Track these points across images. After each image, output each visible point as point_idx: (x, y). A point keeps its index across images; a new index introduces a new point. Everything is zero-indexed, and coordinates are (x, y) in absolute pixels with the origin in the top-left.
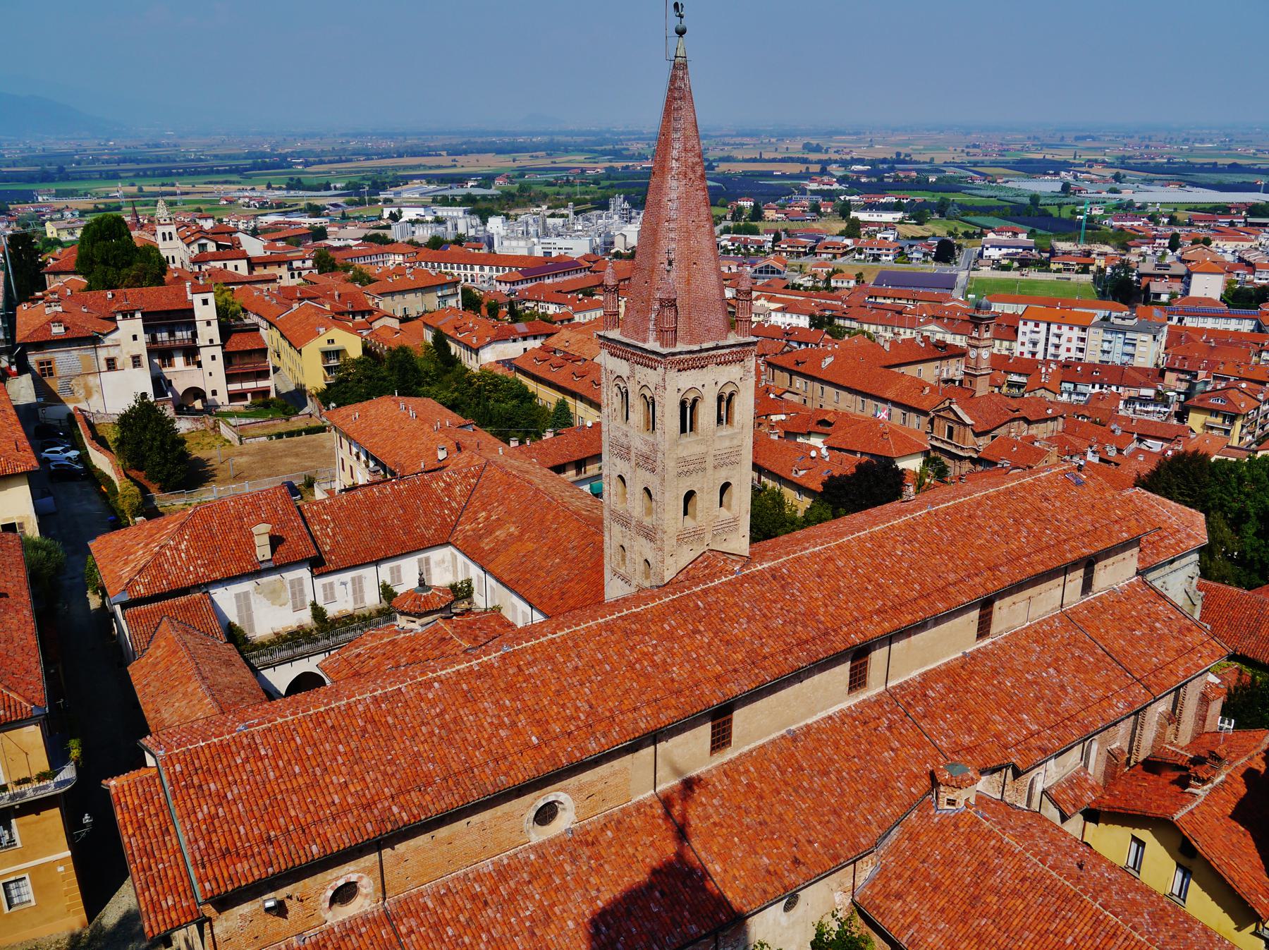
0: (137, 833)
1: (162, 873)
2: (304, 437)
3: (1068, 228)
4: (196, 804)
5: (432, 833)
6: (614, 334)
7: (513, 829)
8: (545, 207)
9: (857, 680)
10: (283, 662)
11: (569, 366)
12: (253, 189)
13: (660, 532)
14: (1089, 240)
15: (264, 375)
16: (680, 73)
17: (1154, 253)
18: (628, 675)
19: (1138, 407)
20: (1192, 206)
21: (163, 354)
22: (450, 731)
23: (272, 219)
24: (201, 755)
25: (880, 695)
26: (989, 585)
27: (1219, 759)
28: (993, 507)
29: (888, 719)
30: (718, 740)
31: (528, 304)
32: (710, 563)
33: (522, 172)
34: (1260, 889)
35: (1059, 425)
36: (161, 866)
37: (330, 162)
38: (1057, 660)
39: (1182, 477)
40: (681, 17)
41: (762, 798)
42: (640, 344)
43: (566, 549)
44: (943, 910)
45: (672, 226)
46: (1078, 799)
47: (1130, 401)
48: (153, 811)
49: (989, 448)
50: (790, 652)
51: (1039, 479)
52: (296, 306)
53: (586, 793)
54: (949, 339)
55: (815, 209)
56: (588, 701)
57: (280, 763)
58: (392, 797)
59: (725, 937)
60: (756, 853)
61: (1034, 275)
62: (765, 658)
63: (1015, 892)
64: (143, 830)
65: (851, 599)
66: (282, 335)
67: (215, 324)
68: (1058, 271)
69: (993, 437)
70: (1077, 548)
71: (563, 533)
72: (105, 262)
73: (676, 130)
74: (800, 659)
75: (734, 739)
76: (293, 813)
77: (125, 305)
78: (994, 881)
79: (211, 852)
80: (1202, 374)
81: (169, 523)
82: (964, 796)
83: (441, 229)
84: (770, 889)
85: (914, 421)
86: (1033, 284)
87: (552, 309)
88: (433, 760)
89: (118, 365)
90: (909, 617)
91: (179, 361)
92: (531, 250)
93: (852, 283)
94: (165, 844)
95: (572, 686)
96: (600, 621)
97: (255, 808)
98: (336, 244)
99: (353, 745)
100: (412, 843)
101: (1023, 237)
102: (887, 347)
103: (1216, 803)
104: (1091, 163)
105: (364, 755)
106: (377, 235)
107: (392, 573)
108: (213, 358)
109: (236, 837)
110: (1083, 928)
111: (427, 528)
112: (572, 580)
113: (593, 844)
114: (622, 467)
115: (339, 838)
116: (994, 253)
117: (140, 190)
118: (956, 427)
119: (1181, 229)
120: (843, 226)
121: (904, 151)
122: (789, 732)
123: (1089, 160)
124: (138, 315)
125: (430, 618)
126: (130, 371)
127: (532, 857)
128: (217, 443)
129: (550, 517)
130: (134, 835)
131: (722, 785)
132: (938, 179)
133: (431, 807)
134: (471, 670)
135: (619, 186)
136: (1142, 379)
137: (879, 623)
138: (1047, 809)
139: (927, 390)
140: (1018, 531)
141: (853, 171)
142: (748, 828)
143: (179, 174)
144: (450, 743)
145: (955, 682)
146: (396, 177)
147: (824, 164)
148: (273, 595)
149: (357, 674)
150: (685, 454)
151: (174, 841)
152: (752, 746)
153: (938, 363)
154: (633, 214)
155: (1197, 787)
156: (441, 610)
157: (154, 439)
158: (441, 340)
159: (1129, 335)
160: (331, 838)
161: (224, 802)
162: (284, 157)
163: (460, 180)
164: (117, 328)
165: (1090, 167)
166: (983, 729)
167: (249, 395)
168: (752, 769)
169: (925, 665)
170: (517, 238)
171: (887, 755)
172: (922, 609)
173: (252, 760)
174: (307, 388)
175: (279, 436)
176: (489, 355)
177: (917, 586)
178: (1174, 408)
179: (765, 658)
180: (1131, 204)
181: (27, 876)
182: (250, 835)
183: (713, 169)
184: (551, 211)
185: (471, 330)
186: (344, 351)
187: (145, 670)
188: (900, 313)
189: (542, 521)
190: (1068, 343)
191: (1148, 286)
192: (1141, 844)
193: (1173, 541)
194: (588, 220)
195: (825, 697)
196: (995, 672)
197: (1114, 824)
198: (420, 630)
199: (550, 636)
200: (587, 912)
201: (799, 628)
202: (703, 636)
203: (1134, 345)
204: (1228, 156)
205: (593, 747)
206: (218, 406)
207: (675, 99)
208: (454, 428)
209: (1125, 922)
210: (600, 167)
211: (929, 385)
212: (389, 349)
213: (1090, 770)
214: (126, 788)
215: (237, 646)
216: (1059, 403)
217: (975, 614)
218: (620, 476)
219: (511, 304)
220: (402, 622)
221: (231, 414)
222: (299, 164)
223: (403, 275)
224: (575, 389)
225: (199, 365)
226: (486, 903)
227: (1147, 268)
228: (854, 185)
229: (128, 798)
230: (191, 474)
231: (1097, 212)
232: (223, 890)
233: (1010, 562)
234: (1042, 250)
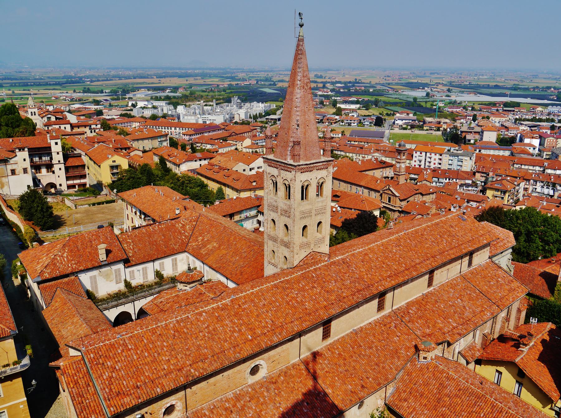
0: (75, 386)
2: (105, 205)
3: (430, 112)
6: (271, 157)
7: (241, 378)
8: (202, 102)
9: (381, 307)
11: (222, 173)
14: (440, 117)
15: (84, 176)
16: (301, 43)
17: (466, 122)
19: (465, 188)
20: (481, 103)
21: (37, 168)
23: (77, 106)
24: (102, 350)
25: (390, 313)
26: (433, 264)
27: (532, 335)
28: (431, 231)
31: (197, 145)
32: (313, 258)
34: (553, 390)
35: (434, 196)
36: (87, 401)
37: (103, 81)
38: (461, 295)
39: (495, 215)
40: (302, 19)
41: (345, 359)
42: (284, 161)
43: (241, 253)
44: (425, 405)
45: (298, 109)
46: (473, 355)
47: (461, 185)
48: (81, 376)
49: (406, 206)
51: (448, 218)
52: (96, 145)
53: (272, 360)
55: (322, 103)
56: (271, 319)
58: (190, 365)
60: (345, 384)
61: (417, 132)
62: (344, 298)
63: (456, 396)
64: (77, 385)
65: (377, 271)
66: (90, 159)
67: (61, 154)
68: (427, 130)
69: (408, 202)
70: (466, 247)
71: (239, 246)
72: (7, 125)
73: (299, 68)
74: (359, 298)
75: (331, 334)
76: (147, 374)
77: (20, 145)
78: (447, 391)
79: (112, 393)
80: (491, 174)
82: (430, 355)
83: (156, 111)
84: (353, 399)
85: (373, 195)
86: (417, 136)
87: (209, 147)
88: (206, 348)
89: (17, 172)
90: (402, 279)
91: (44, 170)
93: (340, 135)
94: (88, 391)
95: (263, 313)
96: (272, 283)
97: (129, 372)
98: (108, 117)
99: (170, 342)
100: (199, 386)
101: (411, 115)
102: (360, 163)
103: (532, 354)
104: (438, 84)
106: (126, 114)
107: (160, 265)
108: (60, 169)
109: (122, 386)
110: (488, 409)
111: (175, 245)
112: (245, 267)
113: (275, 383)
114: (274, 215)
115: (169, 385)
116: (400, 122)
117: (13, 92)
118: (392, 197)
119: (476, 112)
120: (334, 110)
121: (358, 78)
122: (354, 330)
123: (437, 83)
124: (26, 149)
125: (193, 285)
126: (22, 175)
127: (250, 390)
128: (64, 208)
129: (232, 239)
130: (74, 387)
132: (374, 90)
133: (208, 369)
134: (218, 307)
136: (466, 176)
137: (390, 282)
138: (460, 360)
139: (379, 182)
140: (442, 241)
142: (341, 373)
143: (31, 85)
144: (213, 339)
145: (420, 307)
146: (134, 88)
147: (324, 83)
148: (107, 277)
149: (162, 310)
152: (339, 337)
153: (381, 170)
155: (523, 348)
156: (199, 280)
157: (38, 206)
158: (163, 161)
159: (460, 157)
160: (165, 385)
161: (115, 370)
162: (81, 78)
163: (163, 89)
164: (16, 156)
165: (437, 86)
166: (434, 326)
167: (77, 186)
170: (190, 115)
171: (396, 339)
172: (407, 275)
173: (125, 351)
174: (103, 182)
175: (94, 204)
176: (185, 168)
178: (480, 188)
179: (344, 298)
180: (455, 102)
181: (5, 410)
183: (276, 85)
185: (176, 156)
186: (120, 166)
187: (52, 312)
188: (362, 148)
189: (228, 241)
190: (434, 160)
191: (465, 136)
192: (500, 373)
193: (502, 244)
195: (367, 315)
196: (436, 302)
197: (488, 365)
198: (189, 290)
199: (251, 291)
201: (357, 285)
202: (317, 289)
203: (462, 162)
204: (493, 82)
205: (276, 339)
208: (181, 200)
209: (505, 406)
210: (226, 84)
212: (139, 165)
213: (476, 342)
214: (68, 366)
216: (433, 187)
217: (427, 277)
218: (273, 220)
219: (192, 144)
220: (180, 286)
221: (71, 195)
224: (225, 182)
225: (53, 172)
226: (232, 411)
227: (465, 128)
228: (338, 93)
229: (69, 371)
230: (54, 223)
231: (441, 105)
232: (119, 411)
233: (440, 254)
234: (420, 121)
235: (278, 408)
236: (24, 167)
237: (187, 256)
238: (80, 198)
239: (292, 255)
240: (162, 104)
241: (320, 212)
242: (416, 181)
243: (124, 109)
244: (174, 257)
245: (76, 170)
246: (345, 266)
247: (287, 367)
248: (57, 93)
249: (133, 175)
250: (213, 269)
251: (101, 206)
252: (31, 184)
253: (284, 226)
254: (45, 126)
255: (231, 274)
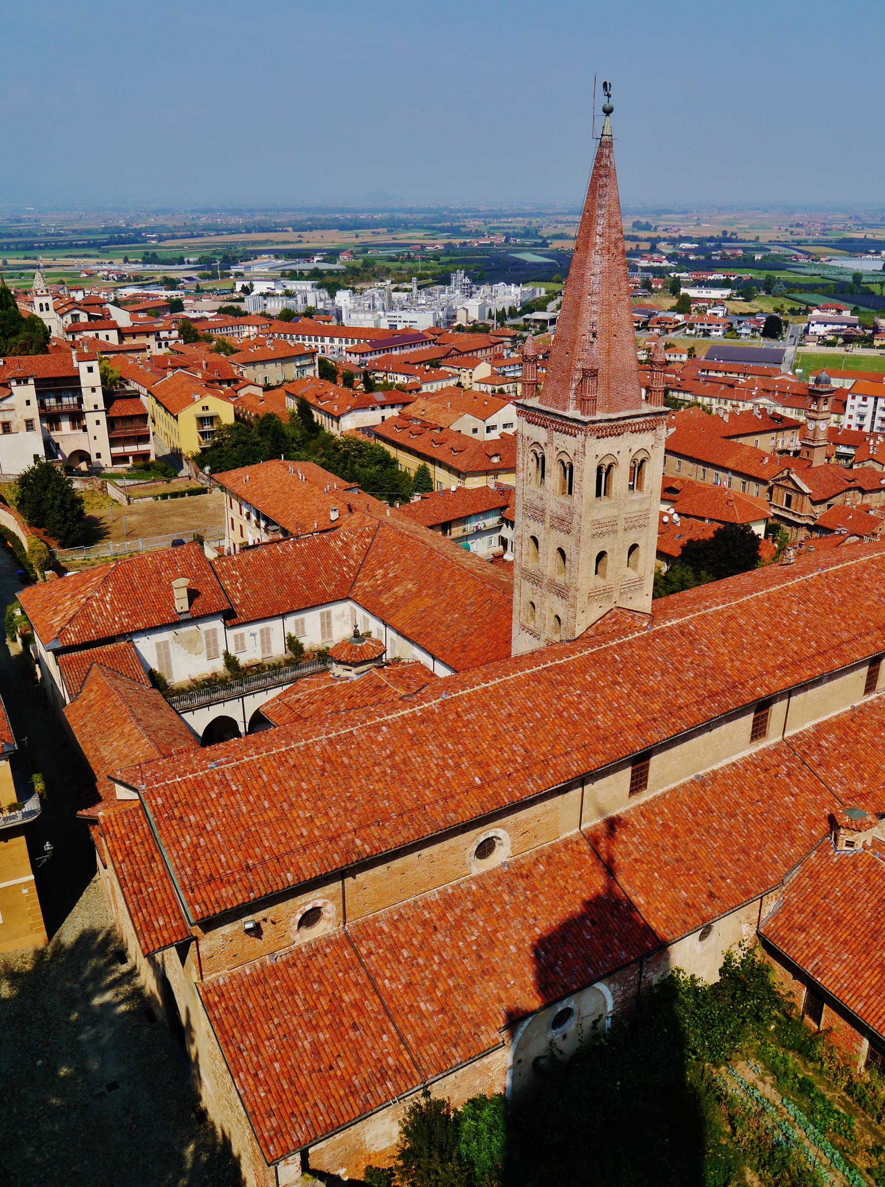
0: (127, 859)
1: (152, 897)
2: (187, 498)
4: (179, 834)
5: (388, 864)
7: (456, 863)
8: (388, 282)
9: (759, 731)
10: (201, 706)
11: (428, 435)
12: (111, 263)
13: (572, 589)
15: (145, 439)
16: (606, 151)
18: (557, 722)
21: (51, 419)
22: (401, 771)
23: (130, 291)
24: (179, 790)
25: (778, 744)
29: (787, 766)
30: (636, 783)
31: (377, 375)
32: (617, 621)
33: (365, 247)
37: (183, 237)
40: (609, 96)
42: (561, 412)
43: (464, 605)
44: (845, 942)
45: (594, 299)
48: (139, 840)
49: (825, 516)
50: (702, 702)
52: (170, 374)
53: (521, 830)
54: (780, 410)
55: (647, 285)
57: (251, 798)
58: (355, 830)
59: (648, 963)
60: (675, 887)
61: (858, 351)
62: (680, 708)
65: (754, 654)
66: (158, 402)
67: (99, 391)
69: (829, 506)
71: (460, 590)
73: (601, 207)
74: (712, 709)
76: (267, 844)
77: (19, 372)
79: (197, 877)
81: (92, 577)
82: (862, 838)
83: (291, 302)
85: (753, 489)
86: (857, 360)
87: (401, 379)
88: (388, 798)
89: (13, 427)
90: (809, 672)
91: (66, 425)
92: (377, 323)
93: (685, 358)
94: (152, 870)
95: (507, 731)
96: (528, 671)
98: (193, 315)
99: (314, 782)
100: (371, 873)
101: (846, 314)
102: (726, 418)
105: (325, 792)
106: (231, 308)
108: (98, 422)
111: (328, 584)
113: (527, 876)
114: (535, 528)
115: (312, 869)
116: (820, 330)
118: (794, 495)
120: (674, 302)
121: (730, 230)
122: (697, 777)
124: (31, 381)
125: (364, 668)
126: (23, 434)
127: (474, 887)
128: (105, 503)
130: (124, 861)
131: (641, 824)
132: (764, 257)
133: (390, 840)
134: (415, 716)
135: (463, 261)
137: (781, 678)
139: (766, 460)
141: (681, 249)
142: (666, 864)
143: (40, 248)
144: (402, 782)
145: (846, 734)
146: (246, 252)
147: (654, 241)
148: (190, 644)
149: (299, 718)
150: (599, 516)
151: (160, 867)
152: (665, 789)
153: (774, 435)
154: (474, 289)
156: (375, 660)
157: (55, 498)
158: (305, 408)
160: (303, 867)
161: (204, 832)
162: (138, 232)
163: (307, 255)
164: (12, 394)
167: (131, 458)
168: (666, 811)
169: (818, 717)
172: (820, 665)
173: (225, 795)
174: (184, 451)
175: (164, 497)
176: (350, 423)
177: (813, 643)
179: (680, 708)
182: (231, 863)
183: (547, 245)
184: (395, 286)
185: (332, 399)
186: (217, 417)
187: (81, 712)
189: (438, 579)
194: (430, 294)
195: (730, 745)
198: (356, 678)
199: (483, 685)
200: (527, 938)
201: (709, 681)
206: (103, 468)
207: (601, 176)
208: (341, 491)
210: (439, 243)
211: (768, 455)
214: (113, 819)
215: (161, 691)
217: (864, 670)
219: (366, 374)
220: (337, 670)
221: (118, 476)
222: (153, 239)
223: (264, 345)
224: (434, 456)
225: (85, 429)
226: (435, 929)
228: (683, 263)
229: (116, 828)
230: (89, 533)
232: (212, 912)
235: (530, 928)
236: (28, 418)
237: (351, 608)
238: (132, 482)
239: (571, 614)
240: (304, 288)
241: (636, 523)
242: (850, 461)
243: (225, 297)
244: (324, 610)
245: (128, 425)
246: (685, 641)
247: (552, 846)
248: (91, 264)
249: (244, 438)
250: (405, 637)
251: (179, 499)
252: (42, 452)
253: (556, 551)
254: (68, 333)
255: (443, 649)
